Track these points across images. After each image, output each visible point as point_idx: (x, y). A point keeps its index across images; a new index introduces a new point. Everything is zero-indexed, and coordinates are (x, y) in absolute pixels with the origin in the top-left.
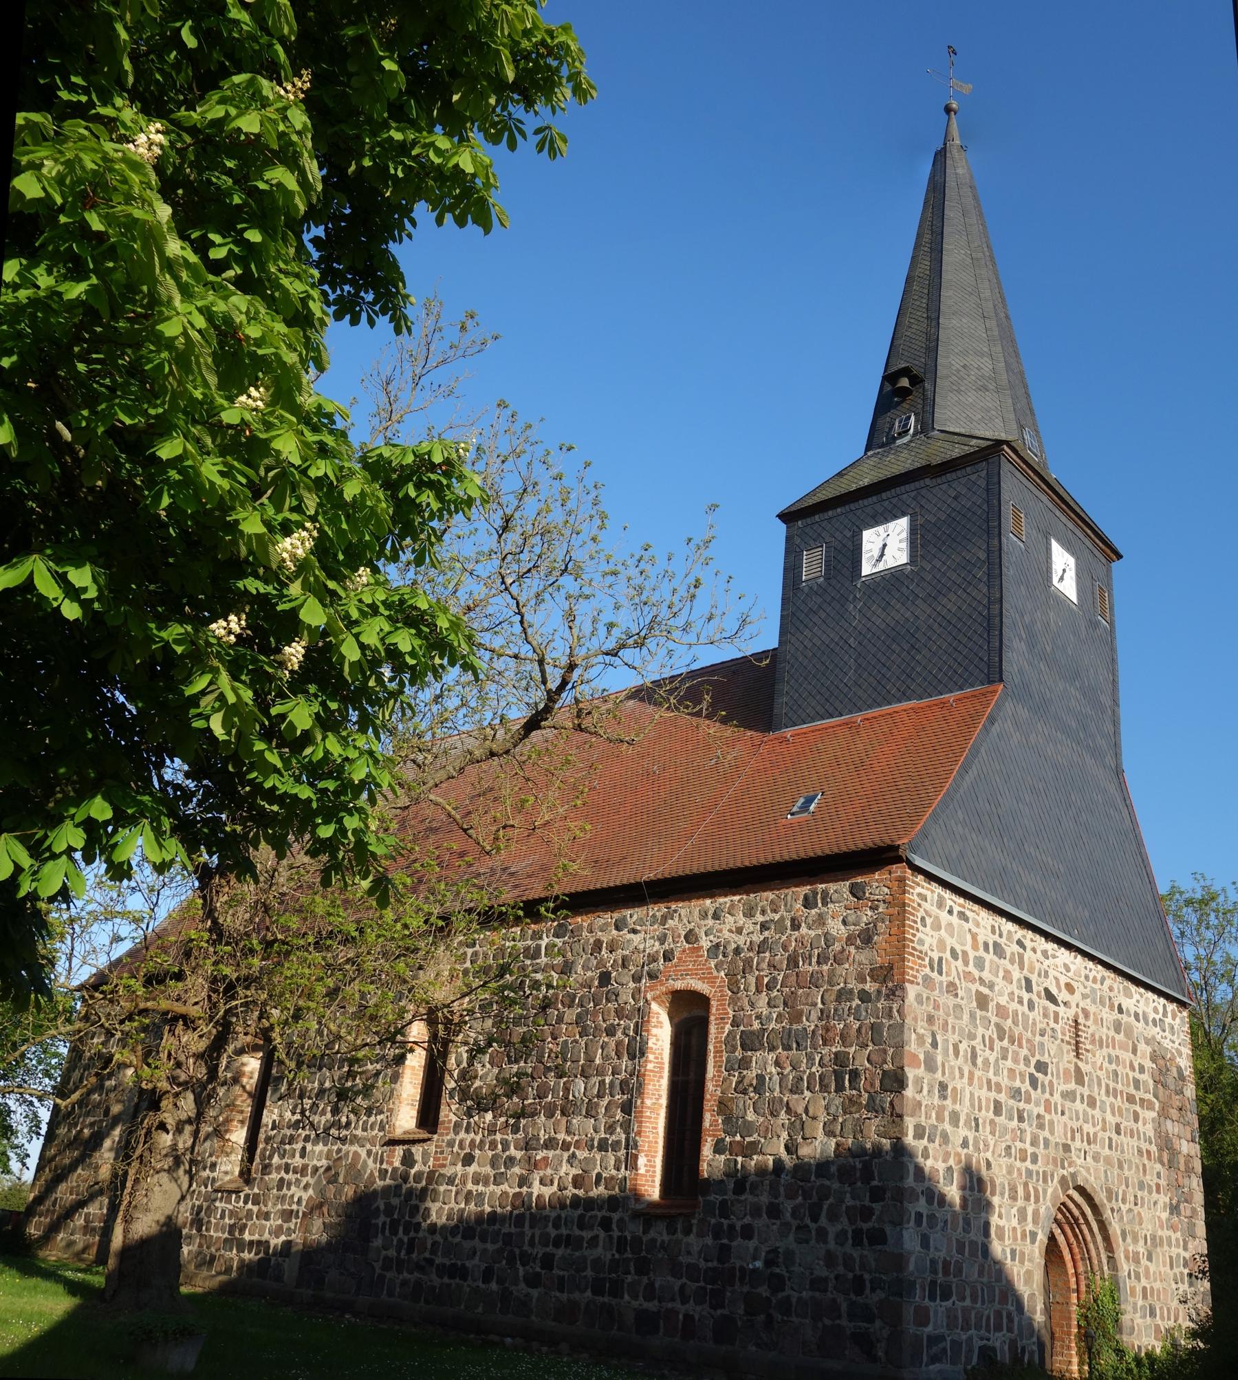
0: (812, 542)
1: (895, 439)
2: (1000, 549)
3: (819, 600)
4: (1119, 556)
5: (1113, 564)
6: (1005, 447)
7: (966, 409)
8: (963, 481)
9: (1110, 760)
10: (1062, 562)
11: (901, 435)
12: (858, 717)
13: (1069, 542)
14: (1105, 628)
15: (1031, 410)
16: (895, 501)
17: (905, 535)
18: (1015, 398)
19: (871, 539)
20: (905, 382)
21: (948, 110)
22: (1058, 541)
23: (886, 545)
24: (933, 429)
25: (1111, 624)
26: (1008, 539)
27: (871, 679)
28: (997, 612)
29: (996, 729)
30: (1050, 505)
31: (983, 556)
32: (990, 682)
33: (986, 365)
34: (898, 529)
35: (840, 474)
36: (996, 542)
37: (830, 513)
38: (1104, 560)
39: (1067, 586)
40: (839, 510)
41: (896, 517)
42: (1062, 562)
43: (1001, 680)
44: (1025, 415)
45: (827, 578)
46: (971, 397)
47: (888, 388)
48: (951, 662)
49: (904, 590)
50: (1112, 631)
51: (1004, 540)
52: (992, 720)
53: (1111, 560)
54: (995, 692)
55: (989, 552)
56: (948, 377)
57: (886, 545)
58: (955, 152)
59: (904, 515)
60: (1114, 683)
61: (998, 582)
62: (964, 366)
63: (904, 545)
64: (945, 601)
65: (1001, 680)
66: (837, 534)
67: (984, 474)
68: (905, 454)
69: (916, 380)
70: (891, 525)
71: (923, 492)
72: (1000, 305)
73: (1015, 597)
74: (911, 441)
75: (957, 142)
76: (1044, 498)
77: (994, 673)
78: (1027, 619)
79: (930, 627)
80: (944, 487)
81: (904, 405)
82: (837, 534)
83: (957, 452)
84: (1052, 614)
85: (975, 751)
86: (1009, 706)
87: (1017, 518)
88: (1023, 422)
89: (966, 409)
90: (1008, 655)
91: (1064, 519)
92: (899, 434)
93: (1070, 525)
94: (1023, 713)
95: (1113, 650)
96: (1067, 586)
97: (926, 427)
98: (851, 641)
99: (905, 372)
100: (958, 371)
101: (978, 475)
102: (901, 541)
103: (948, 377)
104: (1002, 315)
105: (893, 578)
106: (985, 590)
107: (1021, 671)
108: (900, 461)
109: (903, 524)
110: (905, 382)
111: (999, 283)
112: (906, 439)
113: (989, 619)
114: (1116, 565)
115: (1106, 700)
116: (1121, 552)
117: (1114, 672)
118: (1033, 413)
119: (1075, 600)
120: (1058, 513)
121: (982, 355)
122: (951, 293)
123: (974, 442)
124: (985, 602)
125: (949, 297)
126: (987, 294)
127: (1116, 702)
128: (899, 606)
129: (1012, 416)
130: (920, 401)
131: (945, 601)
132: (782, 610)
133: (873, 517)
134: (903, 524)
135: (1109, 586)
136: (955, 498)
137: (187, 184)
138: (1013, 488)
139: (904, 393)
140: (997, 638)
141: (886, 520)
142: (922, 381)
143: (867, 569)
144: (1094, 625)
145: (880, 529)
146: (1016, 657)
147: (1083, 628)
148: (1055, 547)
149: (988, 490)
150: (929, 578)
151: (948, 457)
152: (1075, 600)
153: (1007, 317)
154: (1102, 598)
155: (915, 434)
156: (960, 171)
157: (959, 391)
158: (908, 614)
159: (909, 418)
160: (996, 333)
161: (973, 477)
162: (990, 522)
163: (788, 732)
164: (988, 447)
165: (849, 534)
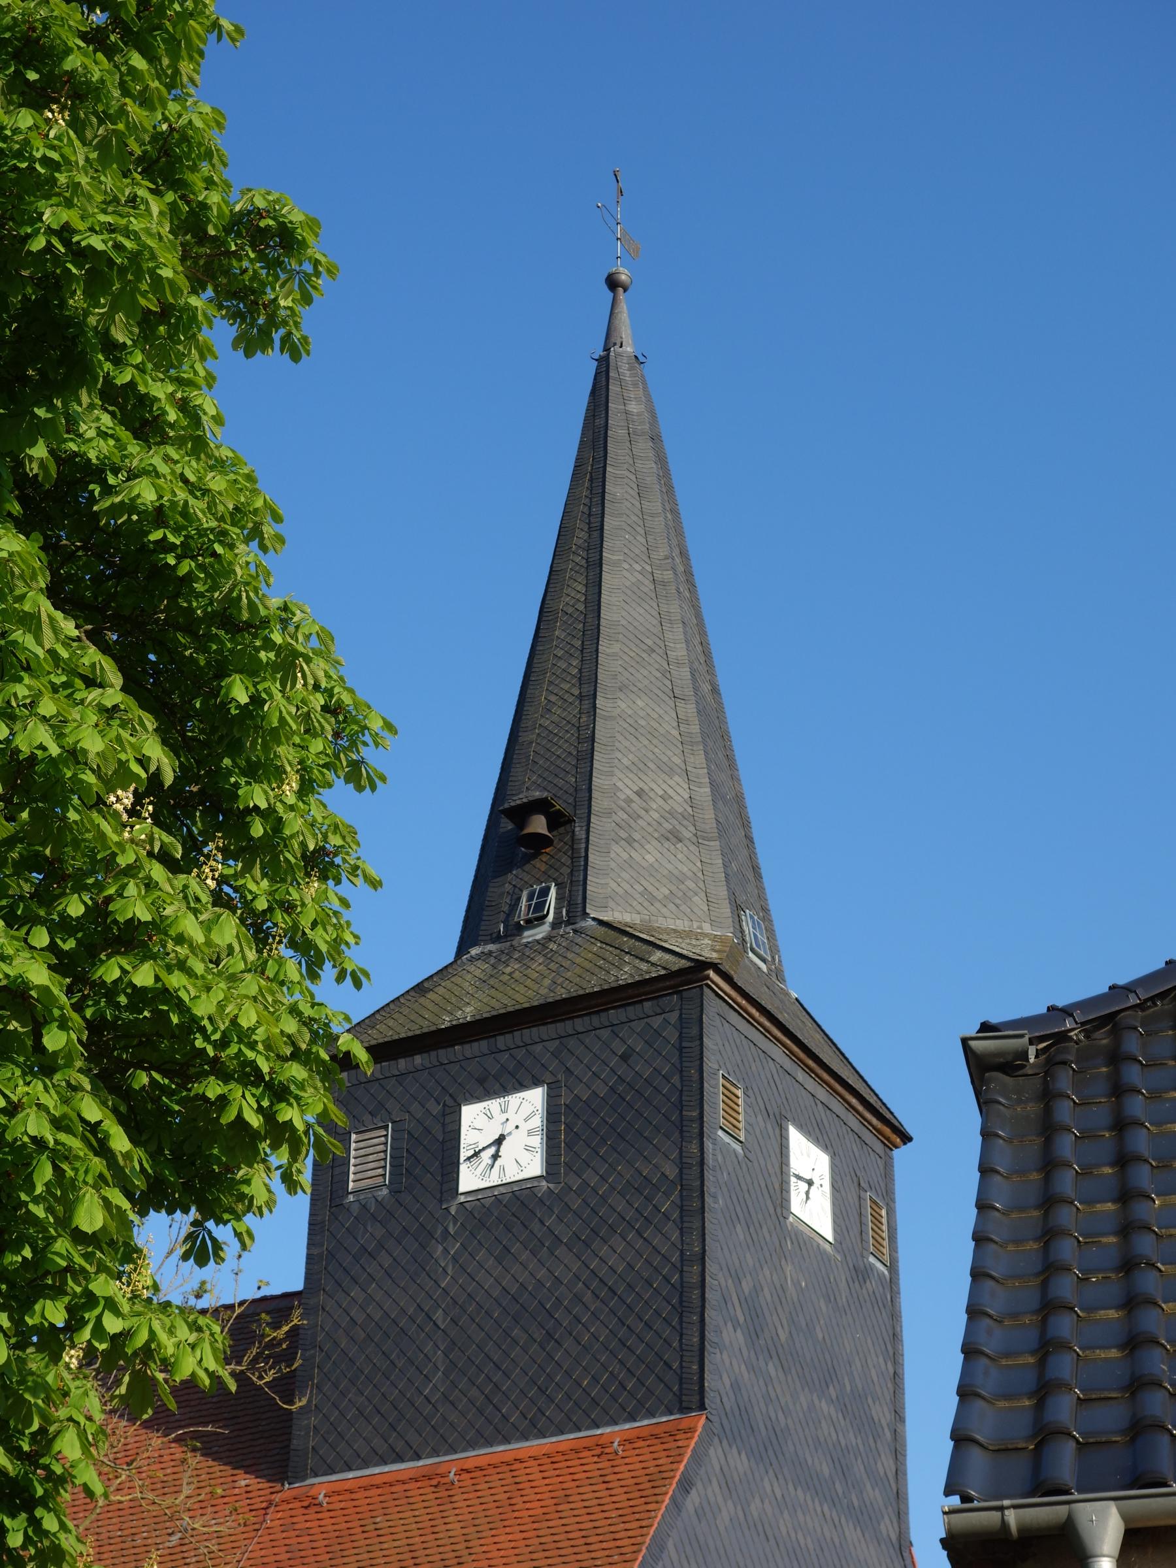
0: (367, 1118)
1: (519, 929)
2: (702, 1163)
3: (379, 1232)
4: (906, 1138)
5: (896, 1153)
6: (711, 973)
7: (645, 882)
8: (638, 1026)
9: (887, 1527)
10: (807, 1158)
11: (530, 923)
12: (450, 1463)
13: (819, 1125)
14: (881, 1276)
15: (756, 869)
16: (520, 1054)
17: (537, 1122)
18: (728, 854)
19: (477, 1121)
20: (538, 825)
21: (613, 283)
22: (801, 1128)
23: (504, 1138)
24: (585, 915)
25: (893, 1267)
26: (715, 1141)
27: (474, 1392)
28: (695, 1279)
29: (693, 1500)
30: (788, 1063)
31: (671, 1171)
32: (684, 1409)
33: (679, 790)
34: (526, 1109)
35: (420, 989)
36: (694, 1148)
37: (402, 1063)
38: (879, 1147)
39: (814, 1210)
40: (418, 1059)
41: (521, 1086)
42: (807, 1158)
43: (702, 1407)
44: (745, 887)
45: (395, 1190)
46: (651, 854)
47: (507, 825)
48: (614, 1367)
49: (535, 1226)
50: (892, 1283)
51: (708, 1145)
52: (686, 1485)
53: (890, 1146)
54: (692, 1430)
55: (682, 1166)
56: (609, 813)
57: (504, 1138)
58: (624, 368)
59: (536, 1083)
60: (897, 1378)
61: (697, 1224)
62: (640, 793)
63: (537, 1141)
64: (604, 1251)
65: (702, 1407)
66: (415, 1107)
67: (673, 1017)
68: (538, 964)
69: (557, 820)
70: (514, 1099)
71: (572, 1043)
72: (703, 669)
73: (730, 1256)
74: (549, 938)
75: (629, 349)
76: (777, 1052)
77: (689, 1395)
78: (747, 1286)
79: (578, 1298)
80: (605, 1034)
81: (536, 862)
82: (415, 1107)
83: (627, 972)
84: (789, 1269)
85: (658, 1546)
86: (715, 1454)
87: (731, 1097)
88: (742, 898)
89: (645, 882)
90: (715, 1359)
91: (810, 1084)
92: (528, 921)
93: (822, 1093)
94: (740, 1463)
95: (895, 1316)
96: (814, 1210)
97: (575, 906)
98: (438, 1315)
99: (541, 806)
100: (629, 801)
101: (663, 1019)
102: (530, 1133)
103: (609, 813)
104: (706, 688)
105: (513, 1202)
106: (675, 1236)
107: (736, 1386)
108: (529, 986)
109: (533, 1099)
110: (538, 825)
111: (701, 625)
112: (539, 933)
113: (682, 1289)
114: (901, 1155)
115: (881, 1413)
116: (910, 1129)
117: (896, 1358)
118: (758, 875)
119: (830, 1238)
120: (801, 1075)
121: (671, 772)
122: (616, 648)
123: (657, 956)
124: (675, 1258)
125: (613, 653)
126: (679, 651)
127: (899, 1416)
128: (525, 1256)
129: (723, 892)
130: (565, 859)
131: (604, 1251)
132: (310, 1244)
133: (481, 1081)
134: (533, 1099)
135: (888, 1195)
136: (624, 1058)
137: (24, 1080)
138: (726, 1041)
139: (539, 843)
140: (696, 1328)
141: (504, 1089)
142: (571, 821)
143: (470, 1179)
144: (862, 1273)
145: (494, 1105)
146: (728, 1362)
147: (843, 1285)
148: (797, 1140)
149: (681, 1049)
150: (576, 1204)
151: (612, 982)
152: (830, 1238)
153: (715, 690)
154: (877, 1219)
155: (555, 925)
156: (633, 407)
157: (630, 841)
158: (542, 1273)
159: (545, 892)
160: (695, 729)
161: (656, 1022)
162: (682, 1110)
163: (320, 1485)
164: (681, 972)
165: (436, 1109)
